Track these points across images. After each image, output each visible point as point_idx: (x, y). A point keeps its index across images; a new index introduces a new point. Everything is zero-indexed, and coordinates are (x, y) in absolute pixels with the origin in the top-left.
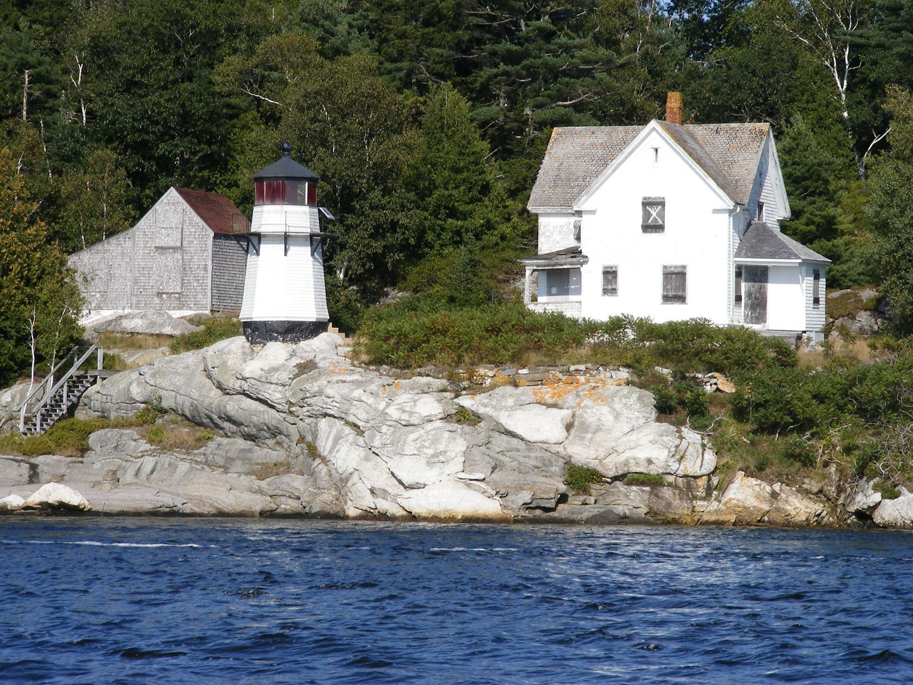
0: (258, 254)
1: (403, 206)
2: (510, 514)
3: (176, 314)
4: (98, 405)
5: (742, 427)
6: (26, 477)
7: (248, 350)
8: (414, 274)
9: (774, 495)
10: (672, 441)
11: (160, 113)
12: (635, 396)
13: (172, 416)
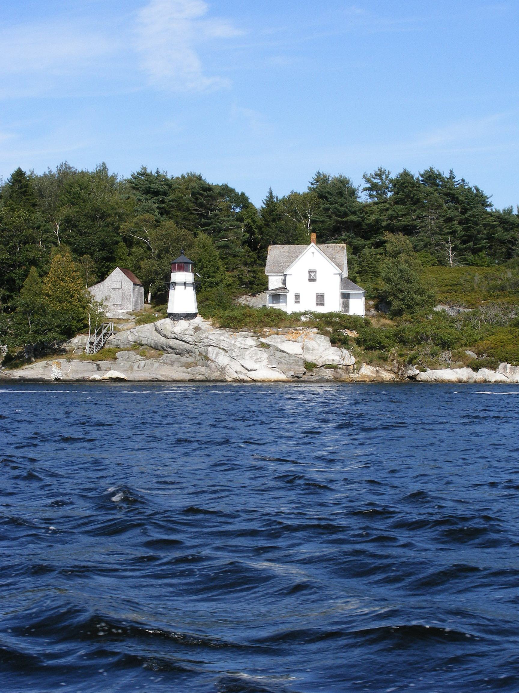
0: (175, 289)
3: (121, 311)
4: (115, 343)
6: (96, 369)
7: (173, 323)
9: (377, 371)
10: (339, 353)
11: (95, 243)
13: (146, 347)
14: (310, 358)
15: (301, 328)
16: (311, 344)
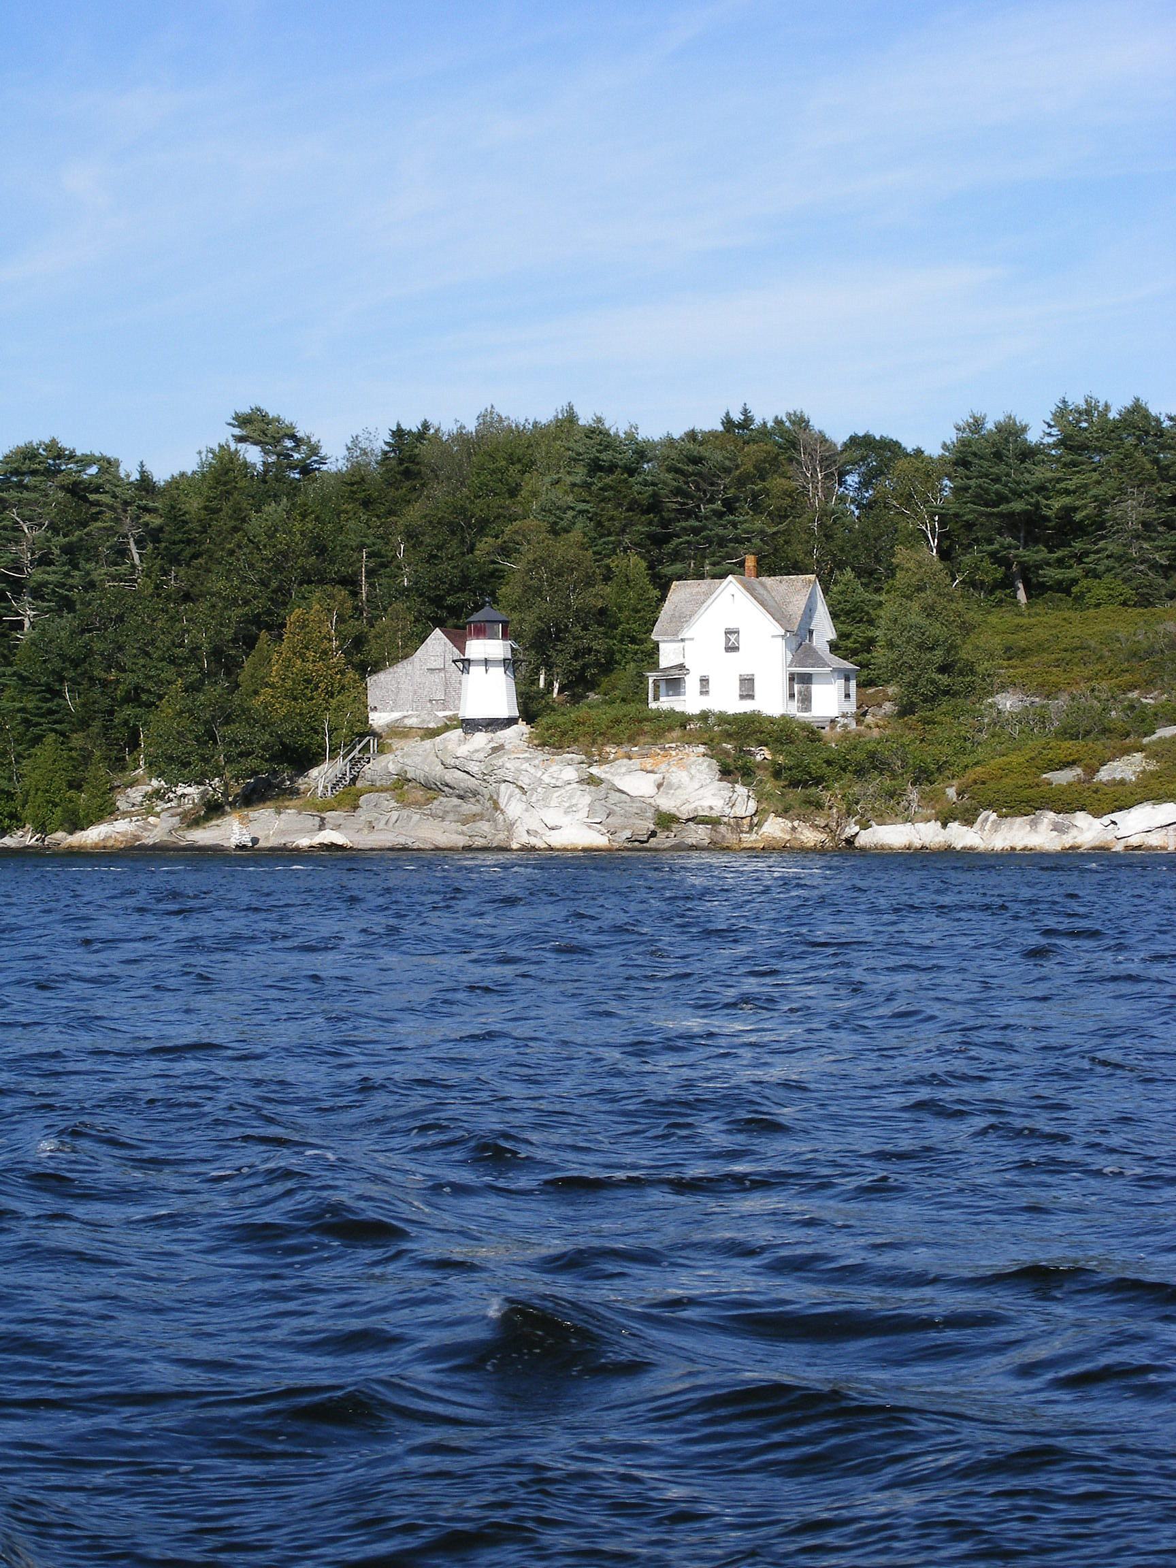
1: (596, 636)
2: (616, 845)
3: (441, 714)
5: (777, 783)
8: (605, 682)
9: (794, 829)
10: (727, 794)
12: (706, 764)
14: (667, 804)
15: (673, 745)
16: (678, 776)
